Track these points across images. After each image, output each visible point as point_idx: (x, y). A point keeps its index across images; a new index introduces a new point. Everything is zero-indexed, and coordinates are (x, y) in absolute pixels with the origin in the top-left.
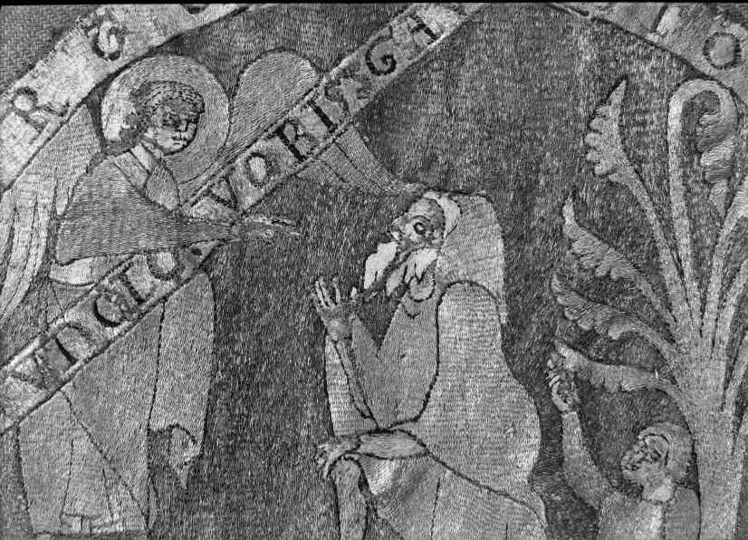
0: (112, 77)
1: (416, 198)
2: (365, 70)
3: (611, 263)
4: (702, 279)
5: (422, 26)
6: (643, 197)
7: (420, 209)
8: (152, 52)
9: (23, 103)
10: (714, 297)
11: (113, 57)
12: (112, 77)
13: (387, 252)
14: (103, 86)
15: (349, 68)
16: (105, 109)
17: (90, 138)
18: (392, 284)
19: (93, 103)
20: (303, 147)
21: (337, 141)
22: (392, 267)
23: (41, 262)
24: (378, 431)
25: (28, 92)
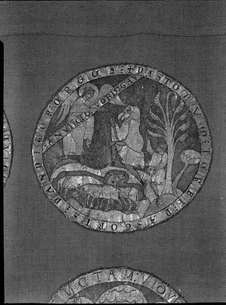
0: (81, 86)
1: (127, 106)
2: (120, 87)
3: (156, 118)
4: (170, 122)
5: (130, 81)
6: (162, 109)
7: (127, 108)
8: (87, 82)
9: (67, 89)
10: (172, 125)
11: (81, 83)
12: (81, 86)
13: (122, 114)
14: (79, 88)
15: (110, 199)
16: (79, 91)
17: (77, 95)
18: (123, 119)
19: (78, 90)
20: (110, 98)
21: (123, 224)
22: (122, 116)
23: (139, 110)
24: (119, 141)
25: (67, 87)
